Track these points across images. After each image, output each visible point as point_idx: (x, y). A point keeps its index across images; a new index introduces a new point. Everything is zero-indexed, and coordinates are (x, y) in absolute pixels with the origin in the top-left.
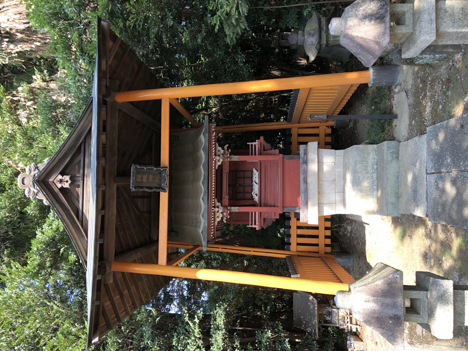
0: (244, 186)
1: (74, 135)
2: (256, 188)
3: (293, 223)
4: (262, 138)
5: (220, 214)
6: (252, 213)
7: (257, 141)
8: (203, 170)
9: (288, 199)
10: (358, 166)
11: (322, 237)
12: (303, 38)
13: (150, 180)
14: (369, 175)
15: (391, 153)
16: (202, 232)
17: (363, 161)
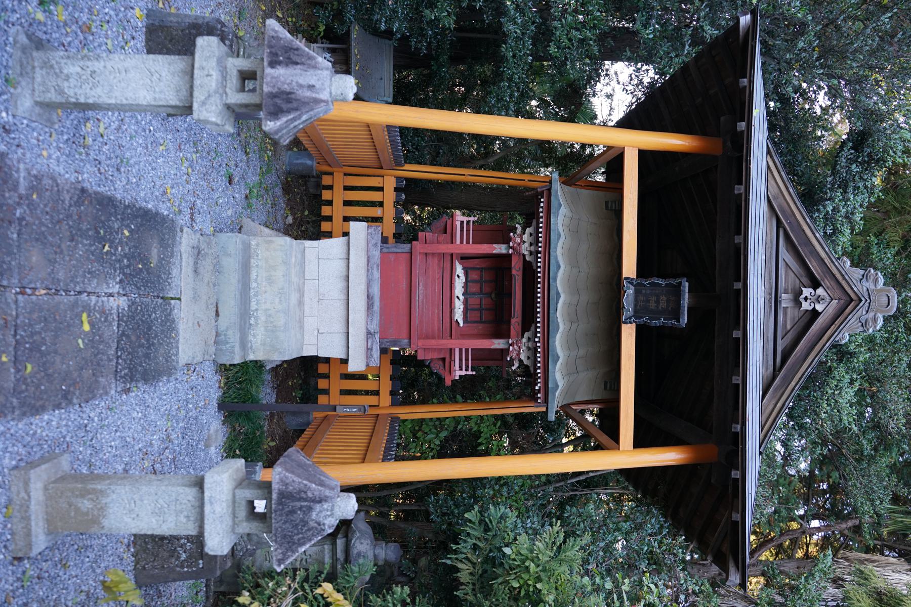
0: (481, 293)
2: (459, 290)
3: (389, 227)
4: (448, 383)
5: (523, 241)
6: (468, 242)
7: (457, 378)
8: (559, 320)
9: (403, 268)
10: (281, 322)
12: (377, 552)
13: (654, 298)
14: (263, 307)
15: (228, 343)
16: (560, 205)
17: (272, 331)
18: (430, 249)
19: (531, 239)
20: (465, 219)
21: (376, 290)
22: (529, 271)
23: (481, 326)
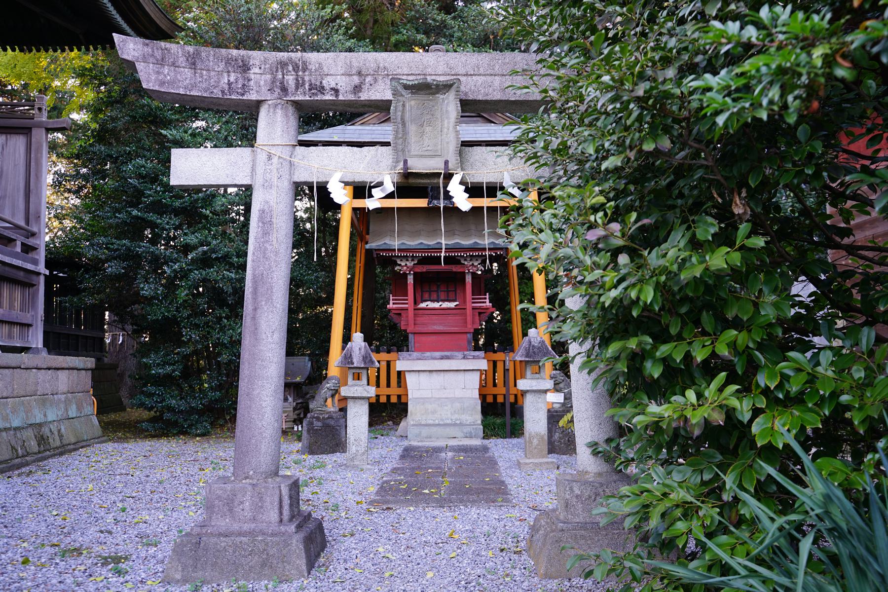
0: (437, 291)
1: (358, 265)
2: (436, 305)
5: (405, 266)
8: (453, 242)
9: (424, 338)
11: (388, 391)
18: (411, 322)
19: (404, 260)
20: (391, 302)
21: (437, 354)
22: (423, 261)
23: (458, 291)
